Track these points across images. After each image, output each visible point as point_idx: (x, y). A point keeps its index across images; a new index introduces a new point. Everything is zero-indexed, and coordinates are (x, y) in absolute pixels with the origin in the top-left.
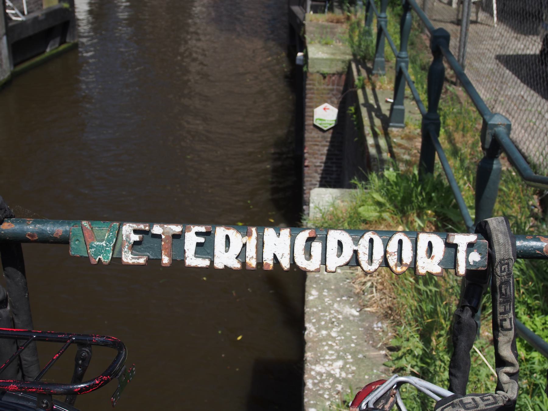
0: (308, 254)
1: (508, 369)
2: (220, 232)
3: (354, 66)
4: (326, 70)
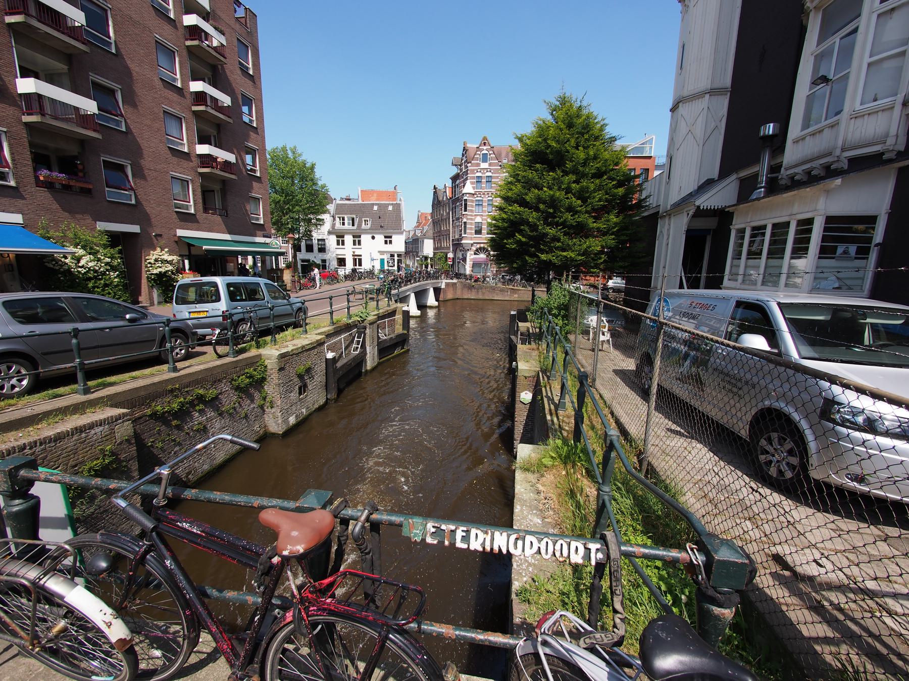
0: (516, 548)
1: (619, 615)
2: (474, 531)
3: (541, 374)
4: (527, 375)
